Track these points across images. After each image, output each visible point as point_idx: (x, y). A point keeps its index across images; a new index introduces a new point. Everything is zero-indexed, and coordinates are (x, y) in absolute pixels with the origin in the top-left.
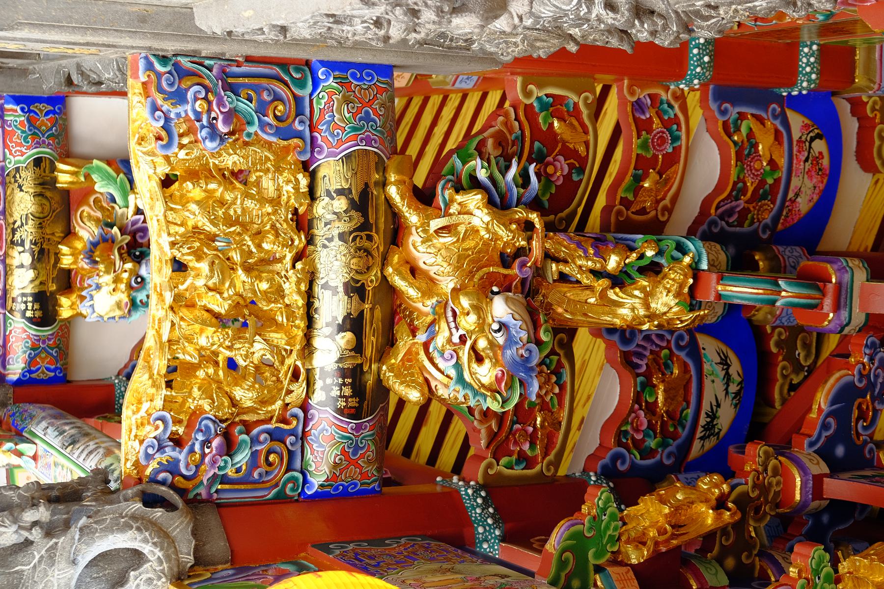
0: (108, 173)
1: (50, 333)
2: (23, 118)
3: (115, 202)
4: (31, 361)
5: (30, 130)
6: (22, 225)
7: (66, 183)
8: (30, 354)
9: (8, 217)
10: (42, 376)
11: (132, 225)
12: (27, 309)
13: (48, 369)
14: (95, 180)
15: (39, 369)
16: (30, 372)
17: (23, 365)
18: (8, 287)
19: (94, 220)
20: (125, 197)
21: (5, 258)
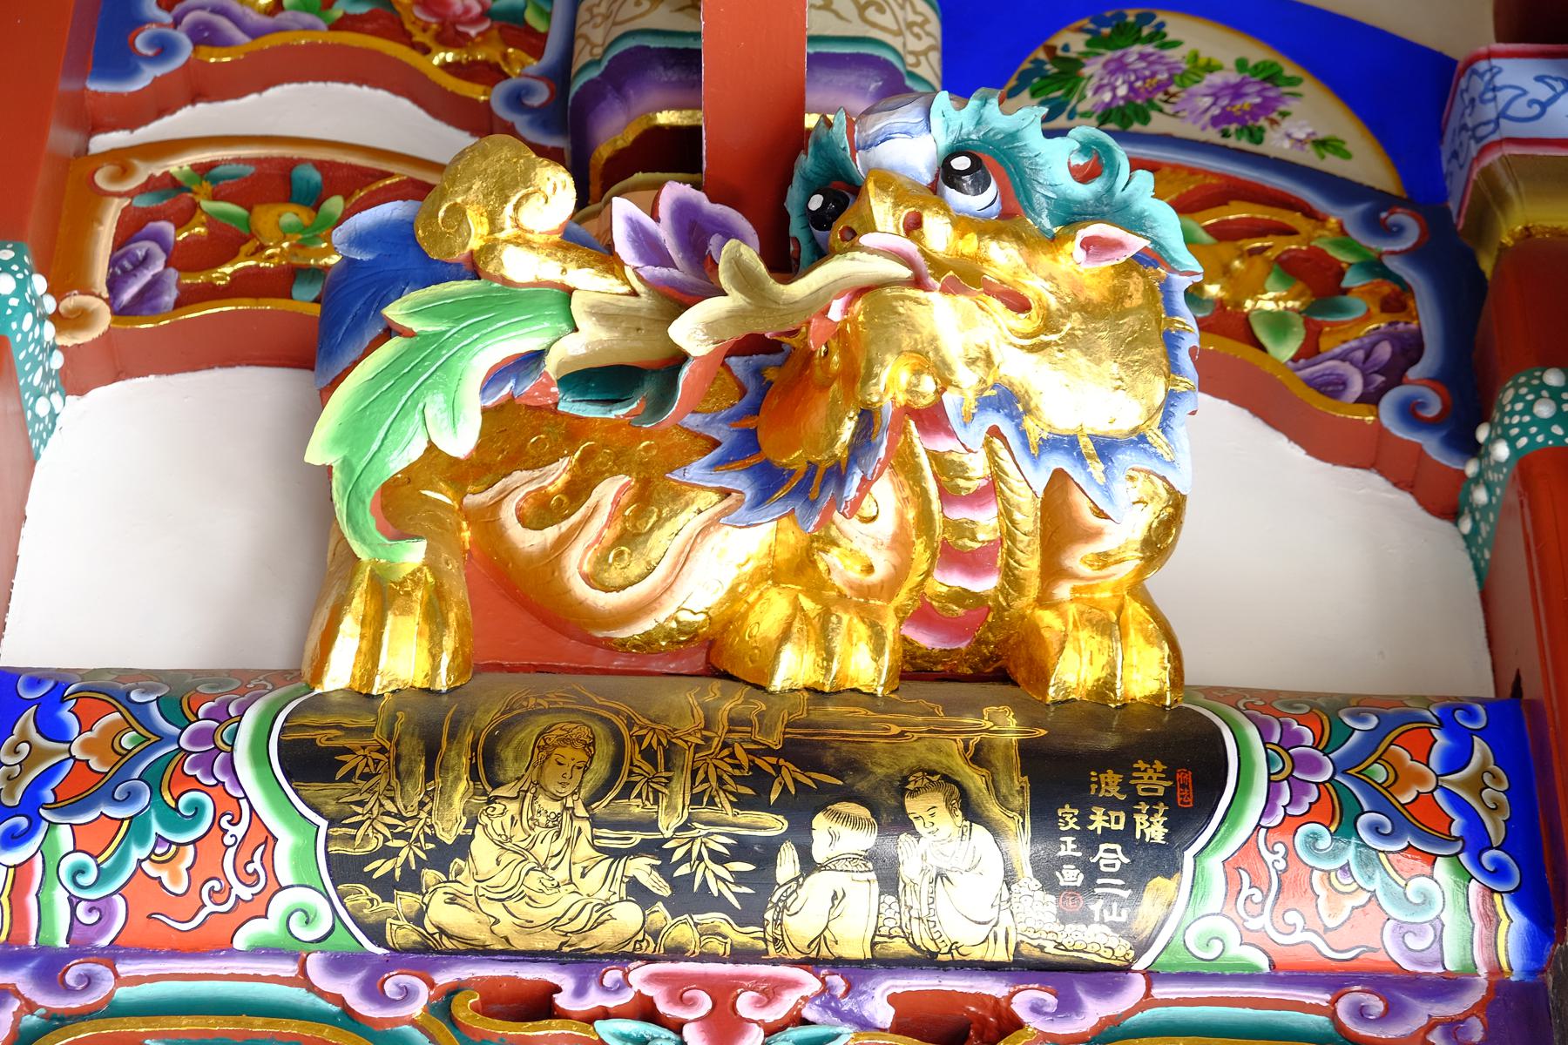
0: (378, 379)
1: (1253, 733)
2: (64, 836)
3: (537, 356)
4: (1418, 829)
5: (131, 796)
6: (653, 848)
7: (435, 657)
8: (1375, 829)
9: (605, 936)
10: (1497, 791)
11: (664, 260)
12: (1126, 838)
13: (1457, 760)
14: (416, 451)
15: (1452, 797)
16: (1476, 841)
17: (1442, 866)
18: (1000, 954)
19: (641, 514)
20: (511, 299)
21: (838, 964)
